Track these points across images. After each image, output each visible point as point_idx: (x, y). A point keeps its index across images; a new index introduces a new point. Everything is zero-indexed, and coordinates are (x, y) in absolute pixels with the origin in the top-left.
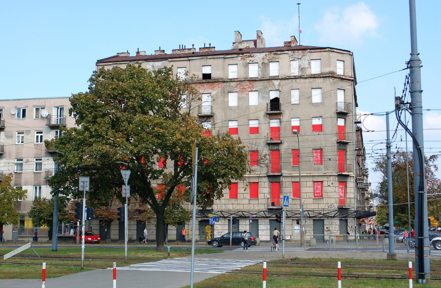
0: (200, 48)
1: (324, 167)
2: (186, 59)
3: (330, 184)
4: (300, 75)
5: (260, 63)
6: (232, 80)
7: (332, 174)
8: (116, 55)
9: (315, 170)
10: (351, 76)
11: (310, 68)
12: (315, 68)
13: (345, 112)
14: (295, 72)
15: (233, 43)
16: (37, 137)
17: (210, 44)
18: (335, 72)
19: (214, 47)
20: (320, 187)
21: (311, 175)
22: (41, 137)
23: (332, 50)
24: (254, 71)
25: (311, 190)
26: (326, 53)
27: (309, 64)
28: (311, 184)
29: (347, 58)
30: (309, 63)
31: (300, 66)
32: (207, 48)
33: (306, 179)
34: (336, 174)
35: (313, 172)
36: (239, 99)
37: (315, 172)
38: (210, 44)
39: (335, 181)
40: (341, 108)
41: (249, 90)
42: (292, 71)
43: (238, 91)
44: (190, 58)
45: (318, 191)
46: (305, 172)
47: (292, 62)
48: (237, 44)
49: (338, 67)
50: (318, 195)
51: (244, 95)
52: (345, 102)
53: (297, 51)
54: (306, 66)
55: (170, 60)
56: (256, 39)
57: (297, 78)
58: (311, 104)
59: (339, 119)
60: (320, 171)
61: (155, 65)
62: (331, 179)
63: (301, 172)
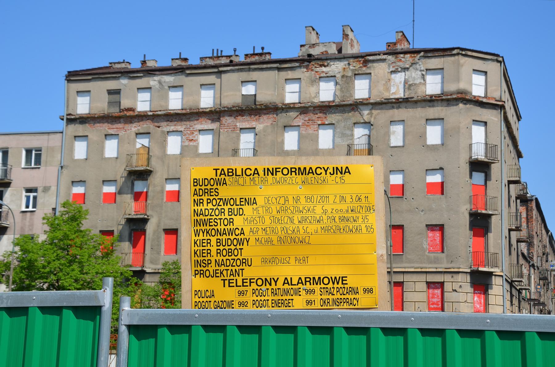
0: (246, 55)
1: (447, 256)
2: (216, 70)
3: (456, 286)
4: (406, 97)
5: (339, 76)
6: (289, 108)
7: (461, 270)
8: (108, 65)
9: (431, 262)
10: (498, 99)
11: (425, 84)
12: (433, 86)
13: (486, 160)
14: (397, 90)
15: (302, 46)
16: (28, 198)
17: (263, 48)
18: (469, 90)
19: (270, 54)
20: (438, 292)
21: (423, 270)
22: (35, 198)
23: (464, 53)
24: (326, 92)
25: (423, 297)
26: (452, 58)
27: (423, 77)
28: (424, 286)
29: (493, 68)
30: (423, 75)
31: (406, 82)
32: (257, 54)
33: (415, 278)
34: (469, 271)
35: (424, 265)
36: (301, 138)
37: (430, 266)
38: (263, 48)
39: (465, 281)
40: (479, 153)
41: (319, 122)
42: (393, 90)
43: (300, 124)
44: (221, 69)
45: (435, 300)
46: (412, 265)
47: (393, 76)
48: (307, 47)
49: (474, 82)
50: (435, 306)
51: (310, 131)
52: (486, 144)
53: (402, 55)
54: (417, 82)
55: (188, 72)
56: (341, 40)
57: (401, 102)
58: (425, 145)
59: (474, 173)
60: (438, 263)
61: (163, 80)
62: (460, 277)
63: (394, 265)
